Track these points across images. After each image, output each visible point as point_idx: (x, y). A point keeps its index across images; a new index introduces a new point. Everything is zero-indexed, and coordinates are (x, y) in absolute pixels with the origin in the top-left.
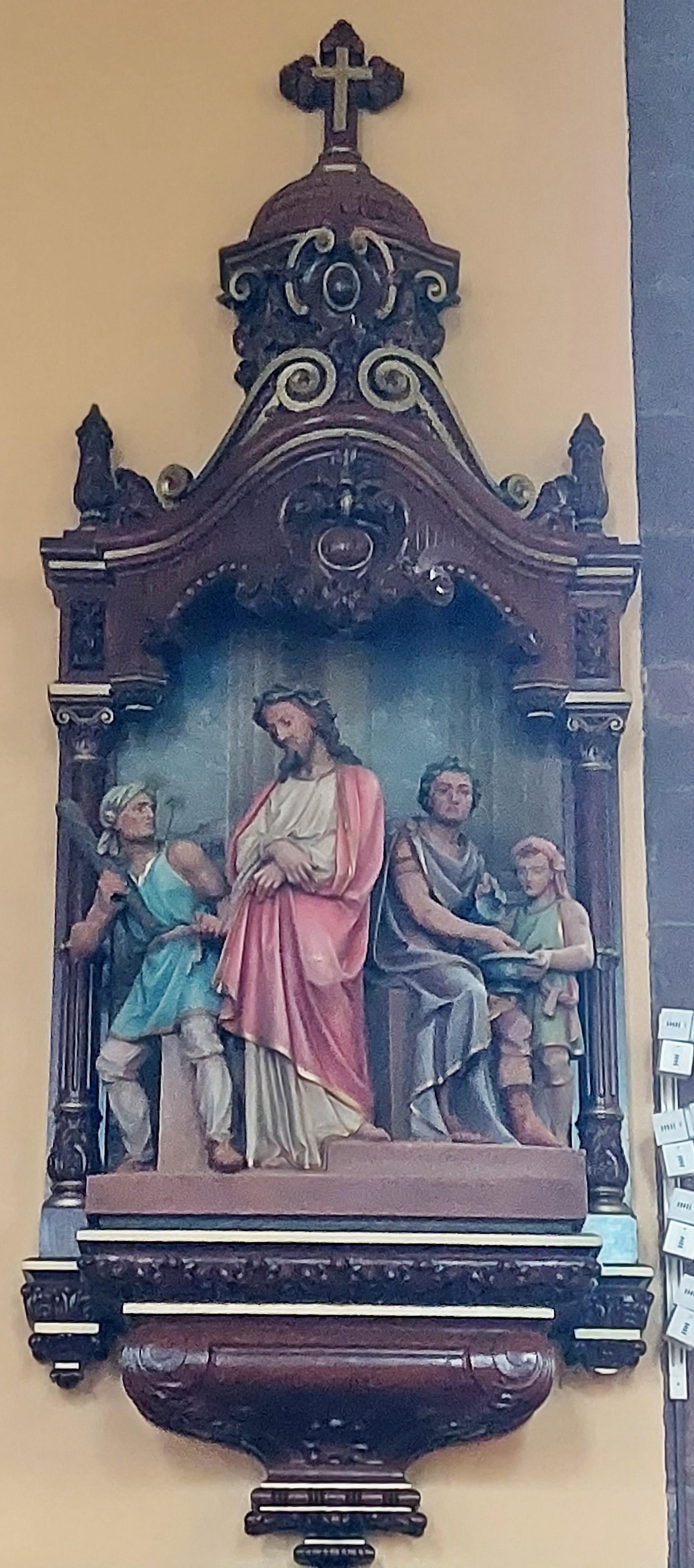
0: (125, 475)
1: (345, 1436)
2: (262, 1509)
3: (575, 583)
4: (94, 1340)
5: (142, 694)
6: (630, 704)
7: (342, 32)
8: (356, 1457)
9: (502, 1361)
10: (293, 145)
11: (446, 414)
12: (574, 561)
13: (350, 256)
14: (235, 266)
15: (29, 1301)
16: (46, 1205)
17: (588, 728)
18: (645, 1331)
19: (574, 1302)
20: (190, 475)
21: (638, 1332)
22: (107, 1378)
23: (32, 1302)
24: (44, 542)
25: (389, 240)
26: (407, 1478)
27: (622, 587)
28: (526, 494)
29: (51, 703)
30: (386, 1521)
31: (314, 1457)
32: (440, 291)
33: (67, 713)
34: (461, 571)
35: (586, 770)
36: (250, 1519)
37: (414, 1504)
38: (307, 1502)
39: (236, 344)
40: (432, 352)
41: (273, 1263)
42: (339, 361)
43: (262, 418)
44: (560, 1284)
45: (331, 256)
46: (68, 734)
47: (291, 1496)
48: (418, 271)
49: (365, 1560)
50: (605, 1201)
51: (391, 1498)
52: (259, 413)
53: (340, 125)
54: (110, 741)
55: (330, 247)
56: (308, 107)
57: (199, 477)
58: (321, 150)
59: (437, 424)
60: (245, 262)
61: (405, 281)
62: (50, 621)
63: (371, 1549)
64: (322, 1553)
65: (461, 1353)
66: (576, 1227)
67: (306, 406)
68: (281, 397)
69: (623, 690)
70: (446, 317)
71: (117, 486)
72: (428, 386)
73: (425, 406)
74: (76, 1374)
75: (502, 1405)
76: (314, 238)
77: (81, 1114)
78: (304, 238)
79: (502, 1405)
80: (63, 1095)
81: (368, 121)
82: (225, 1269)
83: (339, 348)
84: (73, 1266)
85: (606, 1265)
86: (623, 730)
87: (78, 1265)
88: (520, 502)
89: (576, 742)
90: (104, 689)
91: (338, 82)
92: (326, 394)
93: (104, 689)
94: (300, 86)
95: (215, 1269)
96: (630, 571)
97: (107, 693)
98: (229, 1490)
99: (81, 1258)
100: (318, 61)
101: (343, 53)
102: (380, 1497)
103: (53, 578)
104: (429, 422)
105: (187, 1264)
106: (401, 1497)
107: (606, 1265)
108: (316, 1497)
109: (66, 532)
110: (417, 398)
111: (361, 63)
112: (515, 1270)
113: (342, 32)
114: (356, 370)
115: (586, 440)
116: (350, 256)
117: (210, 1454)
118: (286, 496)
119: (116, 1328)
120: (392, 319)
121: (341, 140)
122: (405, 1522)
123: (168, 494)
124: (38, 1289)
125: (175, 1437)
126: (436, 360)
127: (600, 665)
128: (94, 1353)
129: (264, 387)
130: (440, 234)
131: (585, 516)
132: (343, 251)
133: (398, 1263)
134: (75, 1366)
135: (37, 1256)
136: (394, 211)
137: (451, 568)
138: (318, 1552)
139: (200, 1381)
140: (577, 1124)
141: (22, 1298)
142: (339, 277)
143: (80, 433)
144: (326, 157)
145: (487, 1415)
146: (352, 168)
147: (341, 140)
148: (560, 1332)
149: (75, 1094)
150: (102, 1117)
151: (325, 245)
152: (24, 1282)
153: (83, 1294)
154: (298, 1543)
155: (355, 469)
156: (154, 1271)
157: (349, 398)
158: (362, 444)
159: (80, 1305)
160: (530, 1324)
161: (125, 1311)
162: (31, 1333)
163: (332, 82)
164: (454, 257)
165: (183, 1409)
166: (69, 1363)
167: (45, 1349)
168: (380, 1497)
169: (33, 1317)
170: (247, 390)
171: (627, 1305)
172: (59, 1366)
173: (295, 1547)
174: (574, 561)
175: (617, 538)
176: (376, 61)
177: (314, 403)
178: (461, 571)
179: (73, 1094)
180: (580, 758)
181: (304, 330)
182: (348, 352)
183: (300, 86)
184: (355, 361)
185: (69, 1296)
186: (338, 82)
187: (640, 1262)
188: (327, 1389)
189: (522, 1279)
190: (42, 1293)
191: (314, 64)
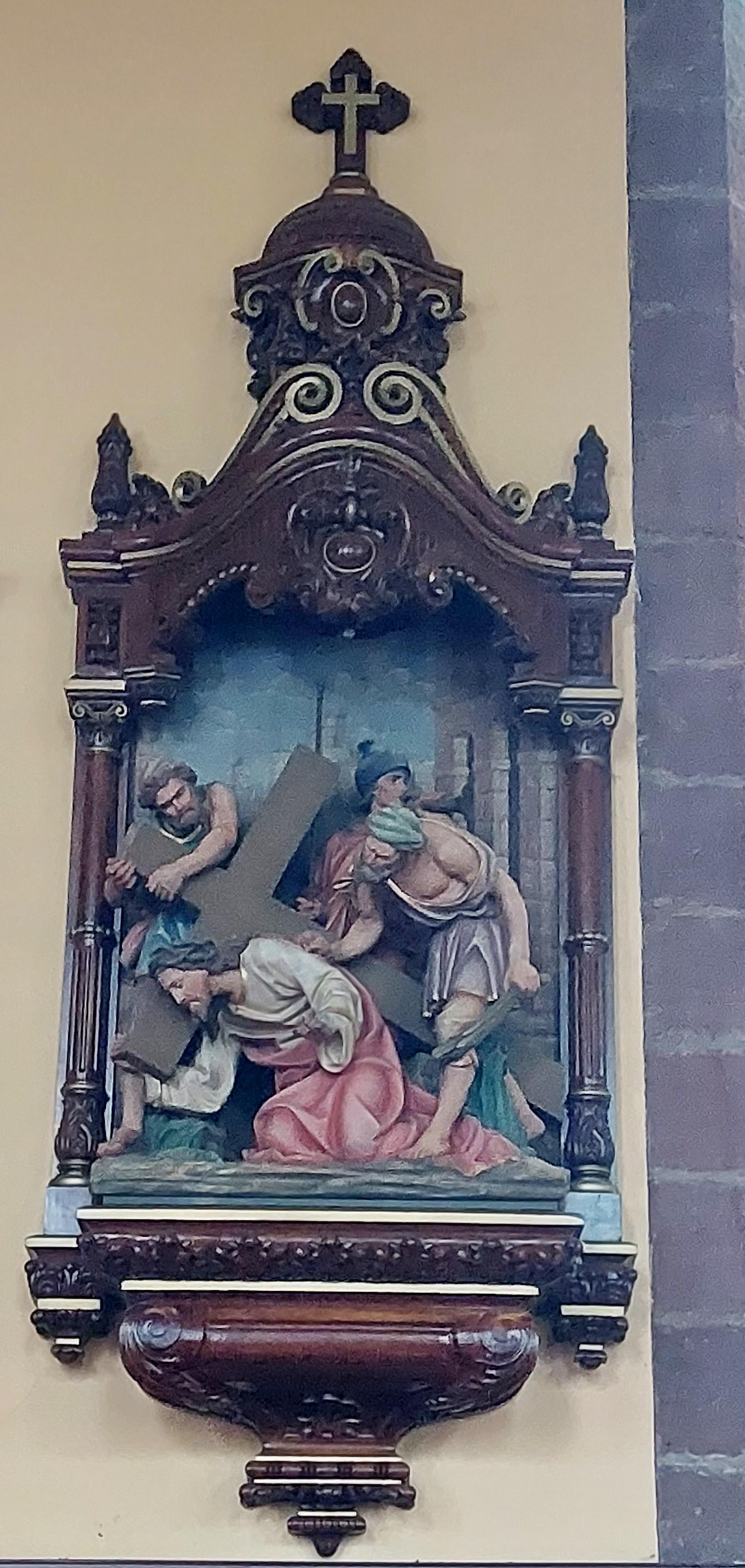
0: (143, 481)
3: (569, 585)
4: (94, 1317)
6: (621, 700)
7: (351, 65)
8: (349, 1431)
9: (487, 1338)
10: (304, 167)
11: (446, 426)
15: (33, 1277)
16: (53, 1183)
17: (583, 723)
18: (630, 1308)
19: (558, 1280)
20: (204, 481)
21: (622, 1308)
22: (107, 1353)
23: (35, 1278)
24: (63, 543)
26: (397, 1452)
27: (611, 590)
29: (67, 697)
30: (377, 1493)
31: (307, 1431)
32: (444, 308)
33: (82, 706)
34: (471, 579)
36: (245, 1491)
37: (404, 1477)
39: (249, 358)
40: (434, 367)
41: (508, 1243)
43: (272, 429)
44: (299, 1258)
45: (340, 276)
48: (424, 288)
49: (357, 1532)
50: (587, 1179)
51: (381, 1471)
52: (268, 425)
53: (350, 148)
54: (127, 734)
56: (320, 131)
57: (212, 483)
59: (438, 434)
60: (259, 281)
61: (409, 298)
62: (66, 617)
63: (363, 1521)
64: (315, 1525)
67: (313, 418)
68: (290, 409)
69: (614, 687)
70: (450, 332)
71: (133, 490)
72: (428, 399)
73: (426, 417)
74: (76, 1350)
75: (487, 1381)
76: (323, 259)
77: (89, 1094)
78: (317, 257)
79: (487, 1381)
80: (71, 1077)
81: (373, 139)
83: (344, 362)
84: (72, 1243)
85: (587, 1242)
86: (613, 726)
87: (78, 1242)
88: (517, 508)
89: (571, 739)
91: (350, 105)
93: (121, 685)
94: (311, 109)
95: (371, 1250)
96: (621, 575)
97: (123, 688)
98: (219, 1464)
99: (80, 1236)
100: (329, 89)
101: (351, 81)
103: (73, 579)
105: (346, 1243)
108: (309, 1470)
109: (84, 535)
111: (369, 90)
113: (351, 65)
114: (361, 382)
115: (591, 452)
117: (207, 1426)
118: (294, 503)
119: (115, 1306)
121: (351, 164)
122: (395, 1495)
123: (183, 500)
124: (41, 1266)
126: (440, 373)
127: (595, 664)
128: (96, 1330)
129: (273, 402)
130: (445, 253)
133: (387, 1241)
134: (76, 1342)
135: (42, 1234)
136: (400, 236)
138: (330, 1523)
139: (193, 1358)
140: (108, 1099)
141: (26, 1275)
142: (344, 292)
143: (101, 440)
144: (335, 182)
146: (361, 191)
147: (351, 164)
148: (545, 1310)
149: (82, 1075)
150: (108, 1099)
151: (333, 266)
152: (29, 1259)
153: (85, 1271)
158: (368, 454)
159: (81, 1281)
160: (446, 1300)
161: (123, 1288)
162: (34, 1309)
165: (187, 1384)
166: (73, 1339)
167: (48, 1324)
168: (264, 1469)
169: (37, 1294)
170: (260, 398)
171: (612, 1282)
172: (60, 1341)
173: (289, 1518)
174: (568, 565)
175: (613, 542)
176: (384, 88)
178: (460, 574)
179: (82, 1075)
180: (574, 753)
181: (313, 345)
182: (354, 366)
183: (311, 109)
184: (361, 376)
185: (71, 1272)
186: (350, 105)
189: (424, 1255)
190: (46, 1270)
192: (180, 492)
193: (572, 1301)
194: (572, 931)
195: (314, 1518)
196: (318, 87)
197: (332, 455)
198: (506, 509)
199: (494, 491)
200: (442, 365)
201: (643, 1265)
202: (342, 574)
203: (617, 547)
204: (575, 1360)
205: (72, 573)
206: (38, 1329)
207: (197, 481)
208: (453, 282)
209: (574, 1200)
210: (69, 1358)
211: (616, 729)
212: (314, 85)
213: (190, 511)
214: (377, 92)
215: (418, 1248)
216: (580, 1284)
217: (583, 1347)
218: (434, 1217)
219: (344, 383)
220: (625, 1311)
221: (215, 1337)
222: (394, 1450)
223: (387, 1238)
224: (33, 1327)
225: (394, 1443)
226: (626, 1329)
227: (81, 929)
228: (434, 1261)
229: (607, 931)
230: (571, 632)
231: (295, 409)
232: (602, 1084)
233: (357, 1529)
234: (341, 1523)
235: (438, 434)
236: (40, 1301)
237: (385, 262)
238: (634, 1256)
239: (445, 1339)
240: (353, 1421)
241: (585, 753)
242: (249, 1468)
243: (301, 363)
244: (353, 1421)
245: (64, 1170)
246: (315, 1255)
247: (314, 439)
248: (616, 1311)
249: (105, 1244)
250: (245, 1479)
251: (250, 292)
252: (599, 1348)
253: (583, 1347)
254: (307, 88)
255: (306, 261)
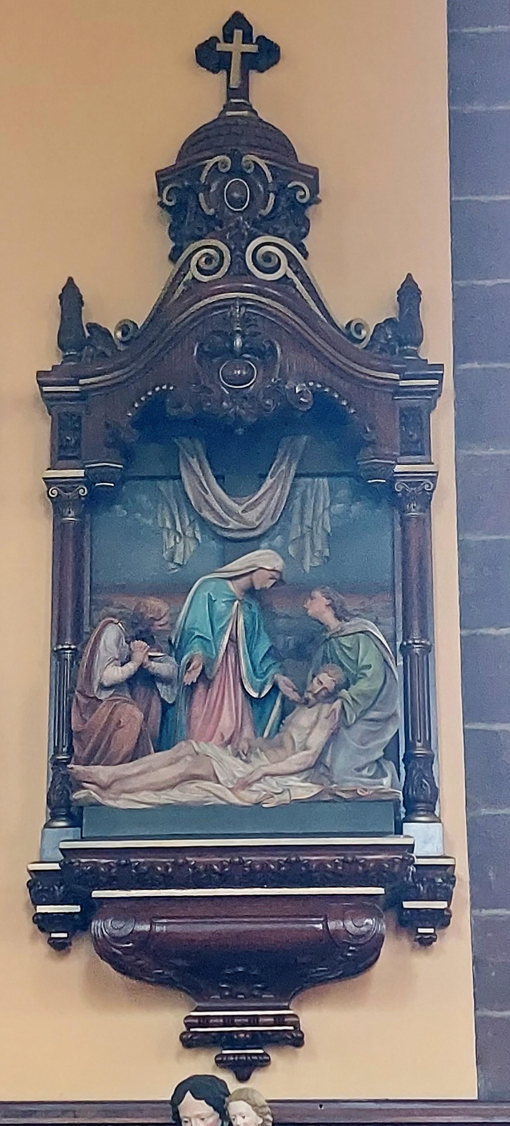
0: (93, 327)
1: (245, 978)
2: (192, 1030)
3: (399, 391)
5: (103, 474)
6: (437, 472)
7: (238, 22)
8: (256, 993)
10: (203, 99)
11: (306, 281)
12: (397, 376)
13: (243, 175)
14: (166, 183)
15: (32, 891)
16: (46, 826)
17: (410, 490)
25: (267, 162)
26: (291, 1008)
28: (364, 332)
31: (227, 993)
35: (409, 519)
36: (184, 1036)
37: (296, 1025)
38: (222, 1025)
42: (233, 247)
43: (181, 288)
46: (58, 505)
47: (211, 1021)
50: (422, 813)
51: (279, 1020)
53: (235, 82)
55: (229, 168)
56: (214, 72)
58: (224, 102)
63: (268, 1055)
65: (322, 919)
66: (399, 831)
69: (433, 464)
70: (310, 212)
71: (87, 334)
73: (291, 275)
76: (217, 163)
78: (211, 163)
80: (56, 752)
81: (253, 75)
82: (159, 866)
83: (231, 238)
84: (56, 866)
85: (418, 857)
86: (432, 491)
87: (60, 866)
89: (403, 502)
90: (81, 473)
91: (239, 52)
92: (224, 269)
93: (81, 473)
94: (209, 56)
95: (152, 867)
96: (436, 382)
98: (168, 1017)
100: (221, 38)
101: (238, 34)
102: (196, 1021)
103: (49, 399)
104: (294, 286)
106: (286, 1020)
107: (418, 857)
108: (229, 1021)
109: (53, 367)
110: (284, 269)
111: (251, 42)
112: (356, 862)
113: (238, 22)
115: (409, 293)
116: (243, 175)
119: (91, 908)
120: (272, 217)
121: (238, 95)
124: (39, 883)
125: (53, 950)
126: (303, 241)
127: (419, 446)
131: (406, 344)
132: (237, 171)
134: (65, 935)
136: (276, 143)
137: (311, 384)
144: (226, 108)
145: (347, 962)
146: (246, 113)
147: (238, 95)
151: (225, 167)
154: (219, 1053)
155: (245, 320)
156: (224, 867)
157: (238, 269)
161: (93, 896)
163: (230, 53)
164: (315, 171)
165: (150, 964)
166: (60, 933)
167: (44, 923)
168: (196, 1021)
172: (54, 935)
174: (397, 376)
175: (426, 360)
176: (262, 40)
177: (215, 276)
178: (319, 386)
181: (212, 225)
183: (209, 56)
186: (239, 52)
187: (447, 855)
188: (231, 947)
190: (40, 886)
191: (219, 42)
192: (119, 334)
193: (411, 898)
194: (405, 638)
195: (234, 1055)
196: (214, 40)
197: (226, 304)
198: (350, 337)
199: (342, 327)
200: (305, 236)
201: (462, 872)
202: (238, 389)
203: (429, 363)
204: (415, 941)
205: (46, 395)
206: (39, 928)
207: (131, 326)
208: (312, 177)
209: (407, 827)
210: (60, 947)
211: (435, 492)
212: (211, 38)
213: (126, 347)
214: (256, 43)
215: (128, 864)
216: (416, 887)
217: (420, 930)
218: (280, 842)
219: (232, 252)
220: (449, 905)
221: (158, 929)
222: (288, 1006)
223: (277, 856)
224: (36, 926)
225: (289, 1001)
226: (451, 916)
227: (60, 647)
228: (253, 871)
229: (431, 639)
230: (402, 424)
231: (198, 272)
232: (428, 745)
233: (264, 1062)
234: (241, 1058)
235: (300, 286)
236: (38, 907)
237: (261, 163)
238: (454, 866)
239: (320, 926)
240: (259, 986)
241: (414, 511)
242: (186, 1021)
243: (200, 238)
244: (259, 986)
245: (54, 816)
246: (227, 869)
247: (274, 297)
248: (442, 905)
249: (79, 866)
250: (184, 1029)
251: (167, 188)
252: (431, 931)
253: (420, 930)
254: (269, 40)
255: (206, 164)
